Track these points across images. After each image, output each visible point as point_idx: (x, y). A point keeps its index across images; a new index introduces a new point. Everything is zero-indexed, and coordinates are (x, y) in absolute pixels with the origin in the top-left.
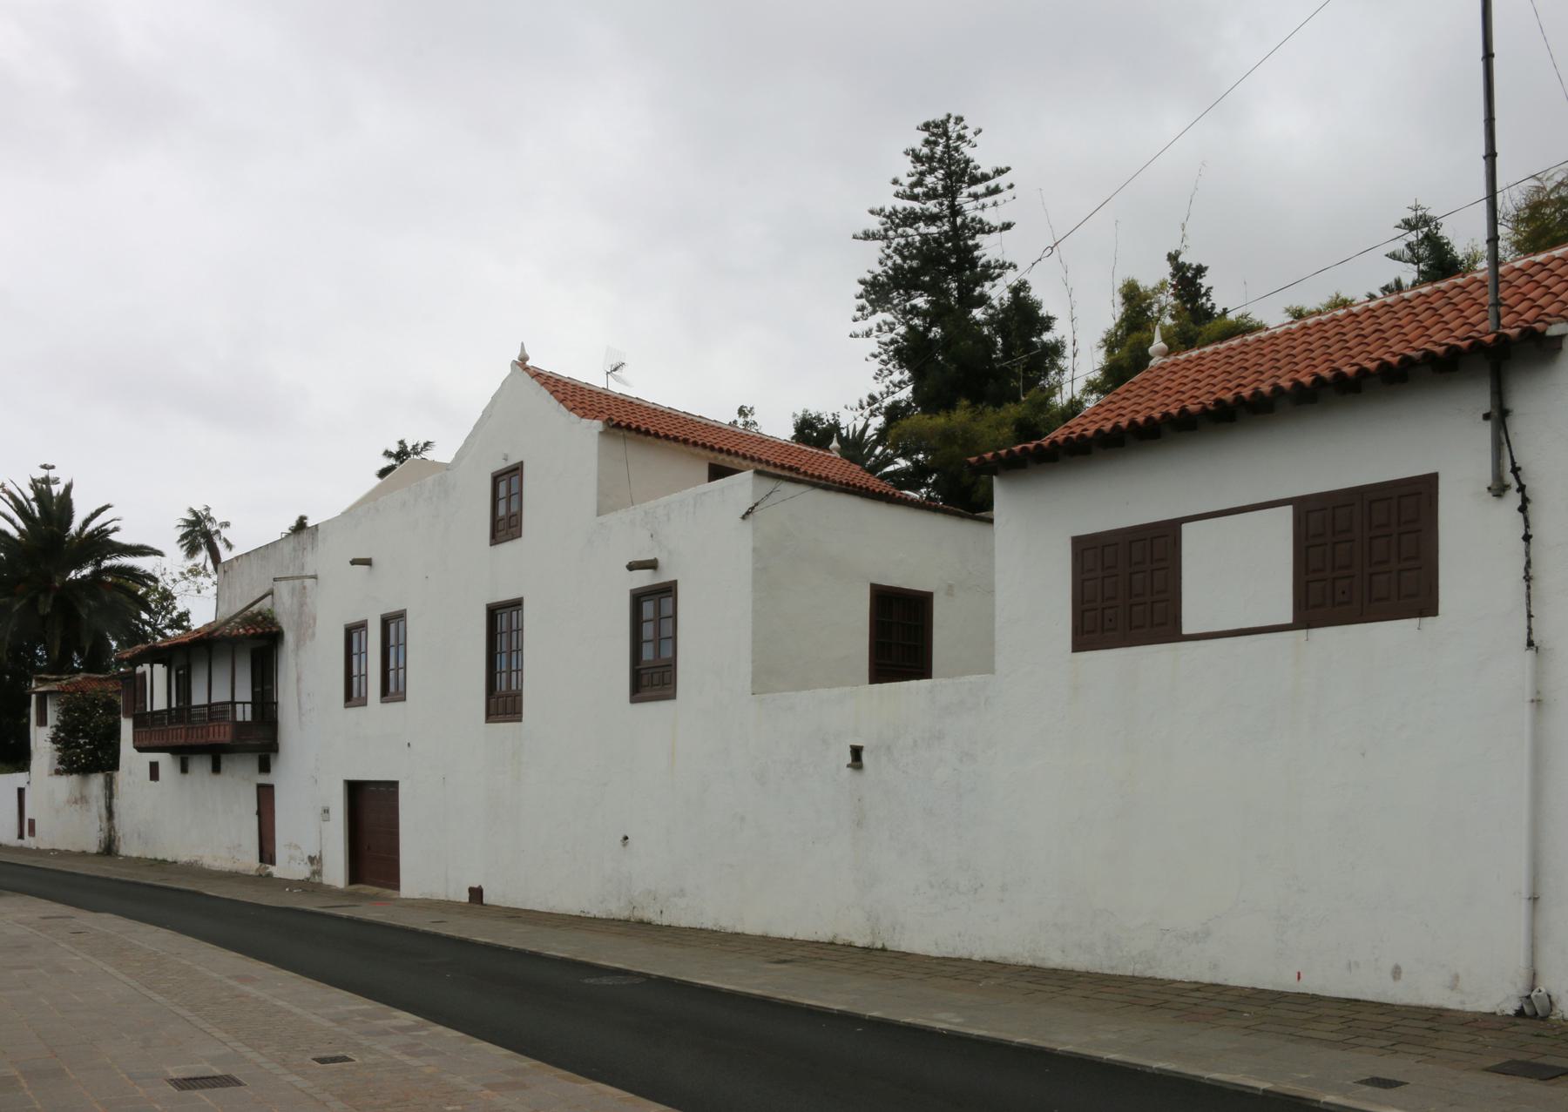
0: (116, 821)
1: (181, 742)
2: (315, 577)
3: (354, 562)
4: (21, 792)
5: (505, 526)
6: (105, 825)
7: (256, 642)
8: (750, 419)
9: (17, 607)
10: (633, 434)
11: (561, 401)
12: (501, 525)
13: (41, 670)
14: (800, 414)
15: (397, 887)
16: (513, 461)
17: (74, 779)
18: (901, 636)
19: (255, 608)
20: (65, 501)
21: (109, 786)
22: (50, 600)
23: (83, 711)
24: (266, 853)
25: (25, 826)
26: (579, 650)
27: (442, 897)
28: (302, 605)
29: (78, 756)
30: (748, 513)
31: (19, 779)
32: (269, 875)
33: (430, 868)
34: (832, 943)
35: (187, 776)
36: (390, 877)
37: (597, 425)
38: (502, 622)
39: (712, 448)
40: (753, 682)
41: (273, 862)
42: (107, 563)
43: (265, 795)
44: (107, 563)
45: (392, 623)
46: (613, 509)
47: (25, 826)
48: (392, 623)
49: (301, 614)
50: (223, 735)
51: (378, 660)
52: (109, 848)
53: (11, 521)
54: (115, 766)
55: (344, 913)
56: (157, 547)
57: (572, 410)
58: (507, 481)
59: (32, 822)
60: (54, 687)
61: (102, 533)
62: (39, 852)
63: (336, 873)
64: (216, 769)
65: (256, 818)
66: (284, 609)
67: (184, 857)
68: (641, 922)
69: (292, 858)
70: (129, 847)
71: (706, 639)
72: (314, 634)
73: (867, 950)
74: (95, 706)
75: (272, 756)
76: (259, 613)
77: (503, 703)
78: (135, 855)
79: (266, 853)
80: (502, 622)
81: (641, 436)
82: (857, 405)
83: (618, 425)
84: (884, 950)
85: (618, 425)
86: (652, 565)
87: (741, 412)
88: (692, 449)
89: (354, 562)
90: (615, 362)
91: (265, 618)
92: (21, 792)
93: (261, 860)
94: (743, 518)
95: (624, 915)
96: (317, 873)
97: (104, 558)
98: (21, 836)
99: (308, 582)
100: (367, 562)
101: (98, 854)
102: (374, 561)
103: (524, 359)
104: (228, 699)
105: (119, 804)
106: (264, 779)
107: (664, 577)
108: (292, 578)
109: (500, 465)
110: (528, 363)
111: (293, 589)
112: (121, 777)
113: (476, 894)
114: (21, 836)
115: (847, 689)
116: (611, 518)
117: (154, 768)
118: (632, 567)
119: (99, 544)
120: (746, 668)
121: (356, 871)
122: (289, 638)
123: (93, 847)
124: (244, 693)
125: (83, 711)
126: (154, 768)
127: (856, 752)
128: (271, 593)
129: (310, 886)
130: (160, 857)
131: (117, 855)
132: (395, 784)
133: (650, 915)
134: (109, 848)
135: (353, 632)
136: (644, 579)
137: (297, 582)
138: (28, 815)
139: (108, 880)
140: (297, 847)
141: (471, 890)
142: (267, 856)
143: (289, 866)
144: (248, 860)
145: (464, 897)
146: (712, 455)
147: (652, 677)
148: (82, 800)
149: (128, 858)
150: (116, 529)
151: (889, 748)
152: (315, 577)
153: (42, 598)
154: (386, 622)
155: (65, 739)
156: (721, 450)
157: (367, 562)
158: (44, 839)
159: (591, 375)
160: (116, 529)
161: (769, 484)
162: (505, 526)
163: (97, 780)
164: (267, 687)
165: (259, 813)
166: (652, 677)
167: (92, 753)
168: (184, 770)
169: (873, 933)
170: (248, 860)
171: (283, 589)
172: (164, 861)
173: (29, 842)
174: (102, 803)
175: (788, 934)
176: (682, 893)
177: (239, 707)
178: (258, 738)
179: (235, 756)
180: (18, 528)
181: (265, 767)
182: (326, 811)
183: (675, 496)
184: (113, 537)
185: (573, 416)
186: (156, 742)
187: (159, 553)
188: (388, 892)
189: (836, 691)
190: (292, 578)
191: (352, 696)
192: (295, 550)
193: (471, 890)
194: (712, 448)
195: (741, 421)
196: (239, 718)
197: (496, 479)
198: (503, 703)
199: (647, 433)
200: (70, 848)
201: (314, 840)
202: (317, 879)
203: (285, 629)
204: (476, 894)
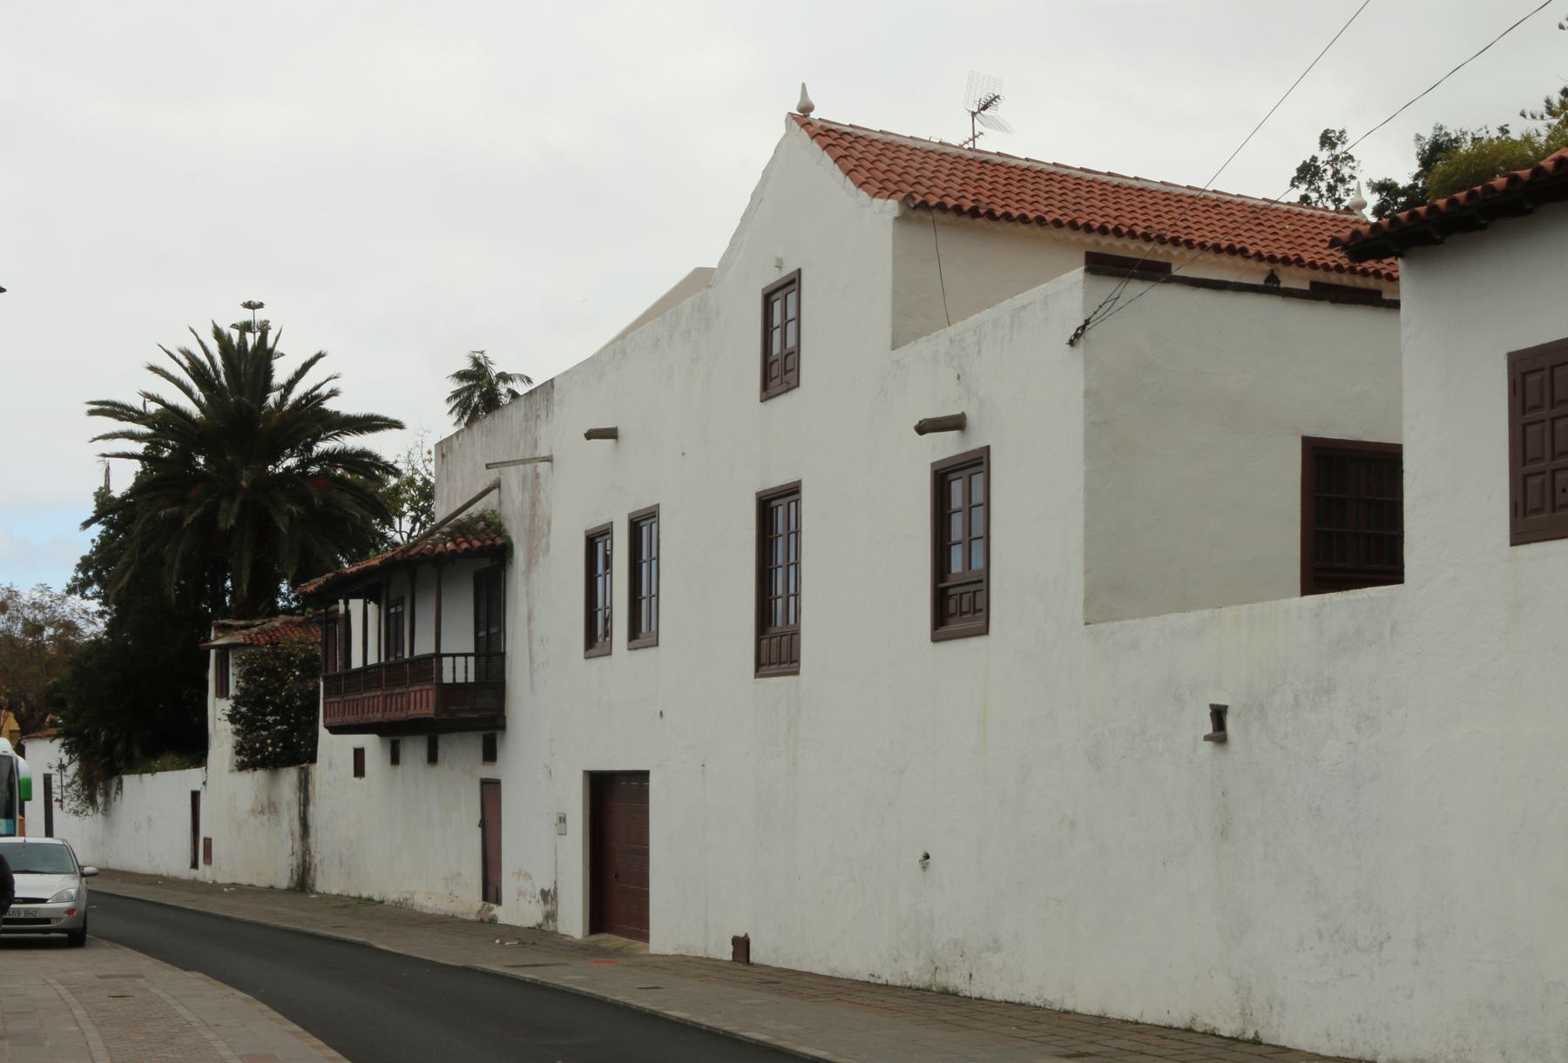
0: (312, 840)
1: (377, 717)
2: (549, 459)
3: (590, 435)
4: (195, 796)
5: (778, 373)
6: (298, 846)
7: (479, 559)
8: (1339, 150)
9: (189, 519)
10: (952, 217)
11: (848, 173)
12: (775, 371)
13: (226, 613)
14: (1428, 135)
15: (645, 937)
16: (789, 269)
17: (260, 775)
18: (1351, 519)
19: (475, 510)
20: (264, 356)
21: (304, 785)
22: (236, 508)
23: (271, 672)
24: (491, 892)
25: (201, 849)
26: (867, 563)
27: (701, 954)
28: (534, 502)
29: (263, 742)
30: (1077, 336)
31: (191, 778)
32: (493, 920)
33: (686, 912)
34: (1189, 1030)
35: (399, 768)
36: (638, 926)
37: (892, 207)
38: (775, 514)
39: (1088, 228)
40: (1088, 603)
41: (498, 901)
42: (321, 447)
43: (491, 791)
44: (321, 447)
45: (642, 525)
46: (916, 336)
47: (201, 849)
48: (642, 525)
49: (533, 516)
50: (422, 703)
51: (625, 580)
52: (303, 881)
53: (188, 392)
54: (313, 759)
55: (528, 975)
56: (392, 416)
57: (861, 185)
58: (782, 295)
59: (208, 842)
60: (238, 638)
61: (312, 400)
62: (214, 888)
63: (573, 920)
64: (433, 758)
65: (479, 831)
66: (513, 509)
67: (392, 895)
68: (945, 993)
69: (521, 893)
70: (329, 882)
71: (1033, 538)
72: (548, 547)
73: (1234, 1040)
74: (289, 665)
75: (499, 734)
76: (482, 517)
77: (776, 647)
78: (335, 891)
79: (491, 892)
80: (775, 514)
81: (966, 220)
82: (1542, 109)
83: (924, 205)
84: (1256, 1042)
85: (924, 205)
86: (956, 423)
87: (1327, 140)
88: (1055, 232)
89: (590, 435)
90: (984, 96)
91: (488, 525)
92: (195, 796)
93: (485, 898)
94: (1071, 343)
95: (920, 978)
96: (551, 916)
97: (316, 439)
98: (195, 865)
99: (543, 467)
100: (611, 434)
101: (289, 889)
102: (621, 432)
103: (806, 109)
104: (432, 650)
105: (317, 813)
106: (488, 772)
107: (974, 443)
108: (523, 462)
109: (773, 277)
110: (814, 115)
111: (525, 477)
112: (319, 771)
113: (741, 946)
114: (195, 865)
115: (1207, 613)
116: (908, 352)
117: (359, 754)
118: (923, 428)
119: (313, 417)
120: (1077, 583)
121: (600, 916)
122: (520, 554)
123: (284, 882)
124: (460, 637)
125: (271, 672)
126: (359, 754)
127: (1219, 714)
128: (497, 485)
129: (541, 938)
130: (365, 895)
131: (312, 892)
132: (643, 776)
133: (955, 980)
134: (303, 881)
135: (595, 541)
136: (947, 446)
137: (529, 467)
138: (203, 834)
139: (266, 927)
140: (528, 876)
141: (735, 941)
142: (492, 890)
143: (518, 909)
144: (469, 900)
145: (726, 953)
146: (1089, 239)
147: (958, 604)
148: (269, 808)
149: (325, 898)
150: (334, 393)
151: (1262, 709)
152: (549, 459)
153: (224, 504)
154: (635, 527)
155: (243, 720)
156: (1103, 230)
157: (611, 434)
158: (225, 869)
159: (939, 123)
160: (334, 393)
161: (1108, 286)
162: (778, 373)
163: (290, 776)
164: (494, 630)
165: (483, 824)
166: (958, 604)
167: (284, 737)
168: (395, 760)
169: (1243, 1014)
170: (469, 900)
171: (512, 478)
172: (370, 900)
173: (205, 873)
174: (295, 813)
175: (1132, 1013)
176: (996, 946)
177: (447, 663)
178: (471, 714)
179: (455, 736)
180: (197, 403)
181: (490, 755)
182: (562, 820)
183: (987, 314)
184: (330, 405)
185: (863, 195)
186: (350, 719)
187: (397, 425)
188: (640, 944)
189: (1192, 617)
190: (523, 462)
191: (595, 637)
192: (526, 418)
193: (735, 941)
194: (1088, 228)
195: (1324, 156)
196: (447, 678)
197: (768, 299)
198: (776, 647)
199: (974, 213)
200: (254, 881)
201: (548, 863)
202: (551, 926)
203: (514, 540)
204: (741, 946)
